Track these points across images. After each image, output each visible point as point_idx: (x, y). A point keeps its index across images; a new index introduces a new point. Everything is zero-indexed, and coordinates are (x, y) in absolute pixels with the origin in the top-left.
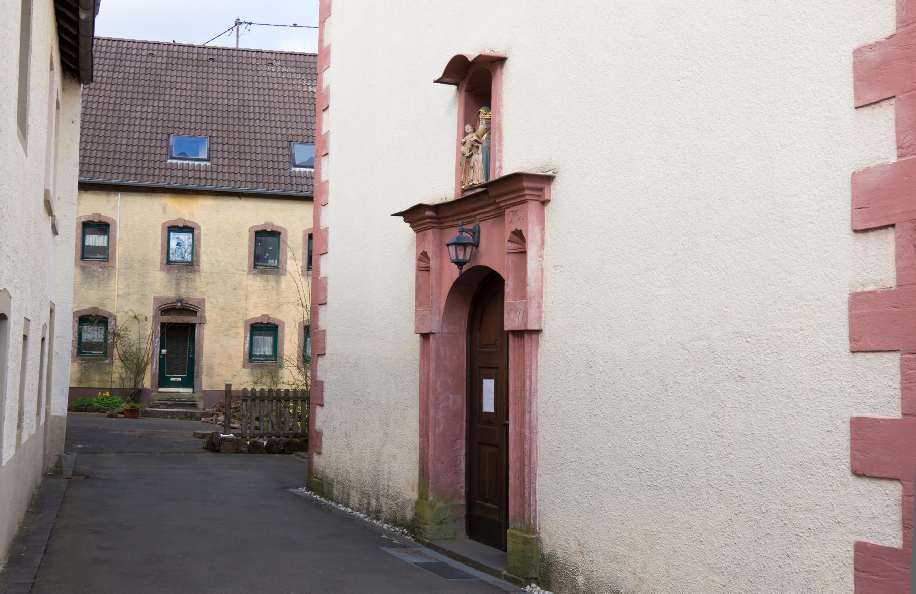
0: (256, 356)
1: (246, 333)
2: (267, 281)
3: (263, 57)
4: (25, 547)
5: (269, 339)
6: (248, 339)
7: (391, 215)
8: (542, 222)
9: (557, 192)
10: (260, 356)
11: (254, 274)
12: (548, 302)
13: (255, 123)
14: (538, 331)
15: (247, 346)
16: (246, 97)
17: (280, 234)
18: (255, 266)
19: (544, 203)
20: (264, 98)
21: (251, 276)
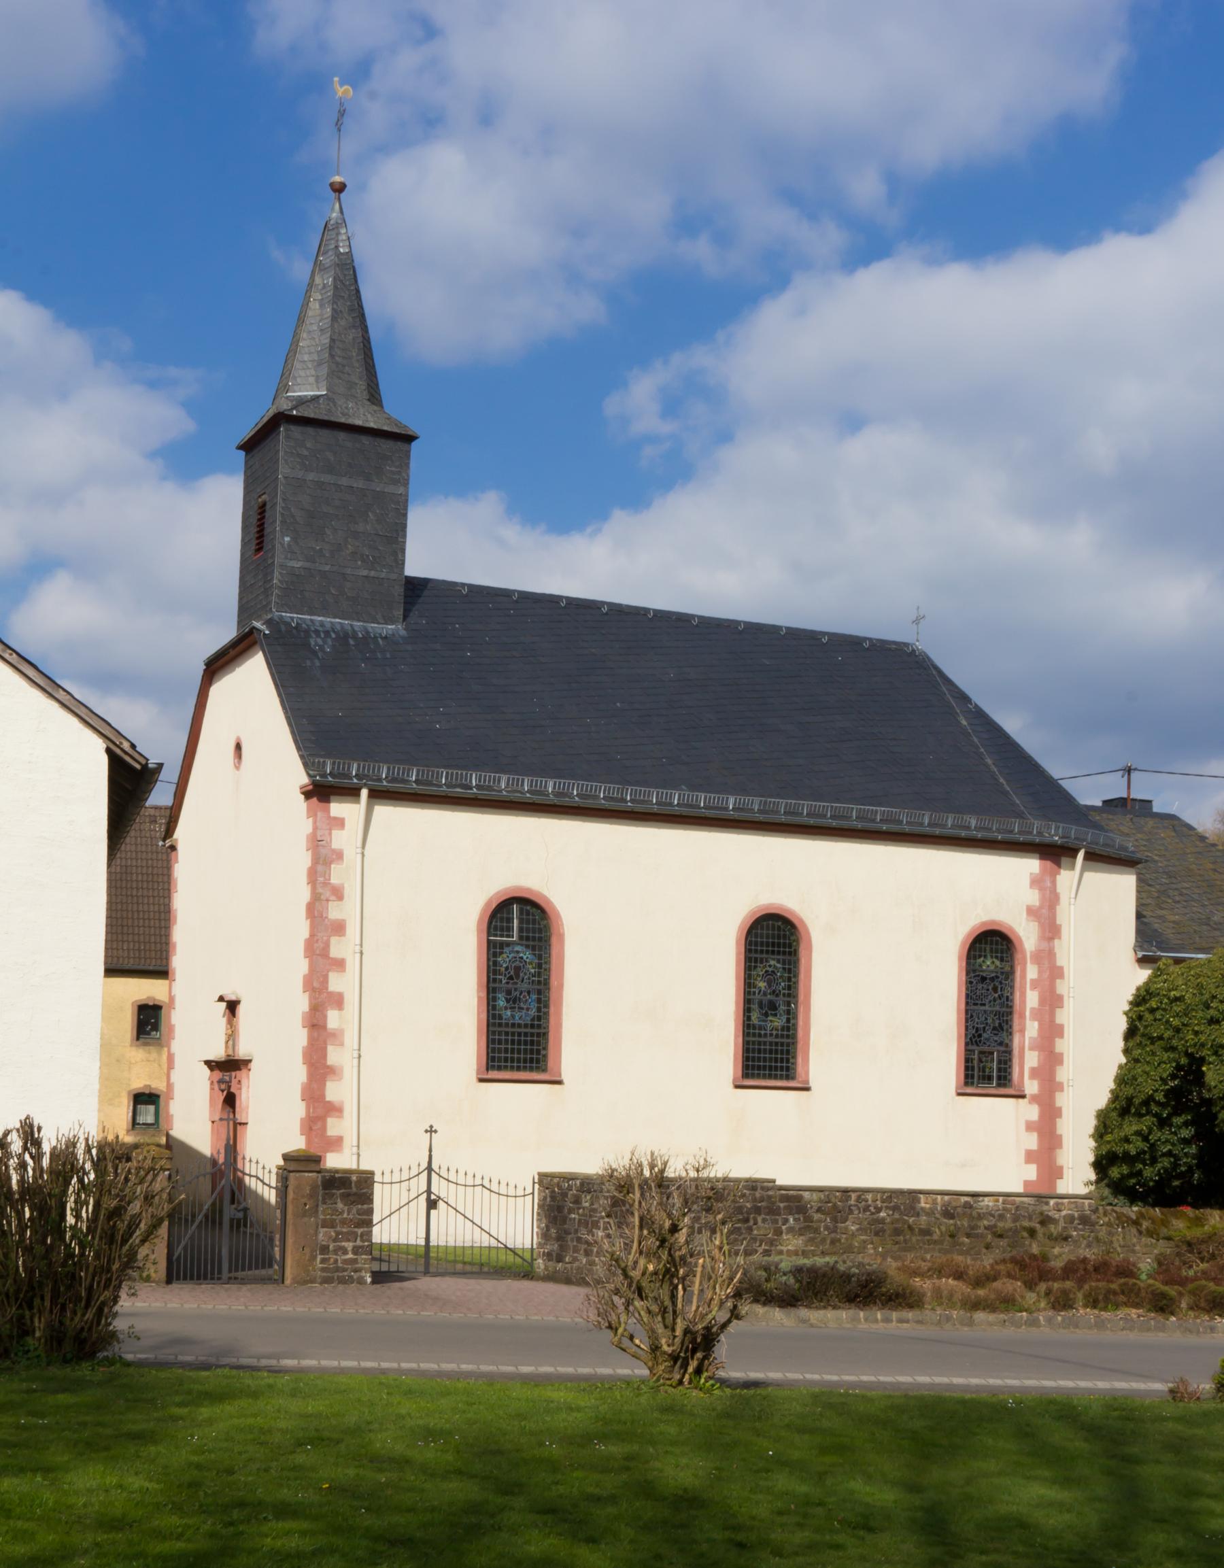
0: (139, 1124)
1: (129, 1103)
2: (149, 1053)
3: (147, 814)
4: (703, 1222)
5: (152, 1108)
6: (131, 1108)
7: (237, 767)
8: (248, 1077)
9: (253, 1065)
10: (143, 1124)
11: (137, 1046)
12: (250, 1110)
13: (138, 892)
14: (247, 1124)
15: (130, 1114)
16: (129, 862)
17: (158, 1096)
18: (138, 1039)
19: (250, 1070)
20: (147, 863)
21: (134, 1048)
